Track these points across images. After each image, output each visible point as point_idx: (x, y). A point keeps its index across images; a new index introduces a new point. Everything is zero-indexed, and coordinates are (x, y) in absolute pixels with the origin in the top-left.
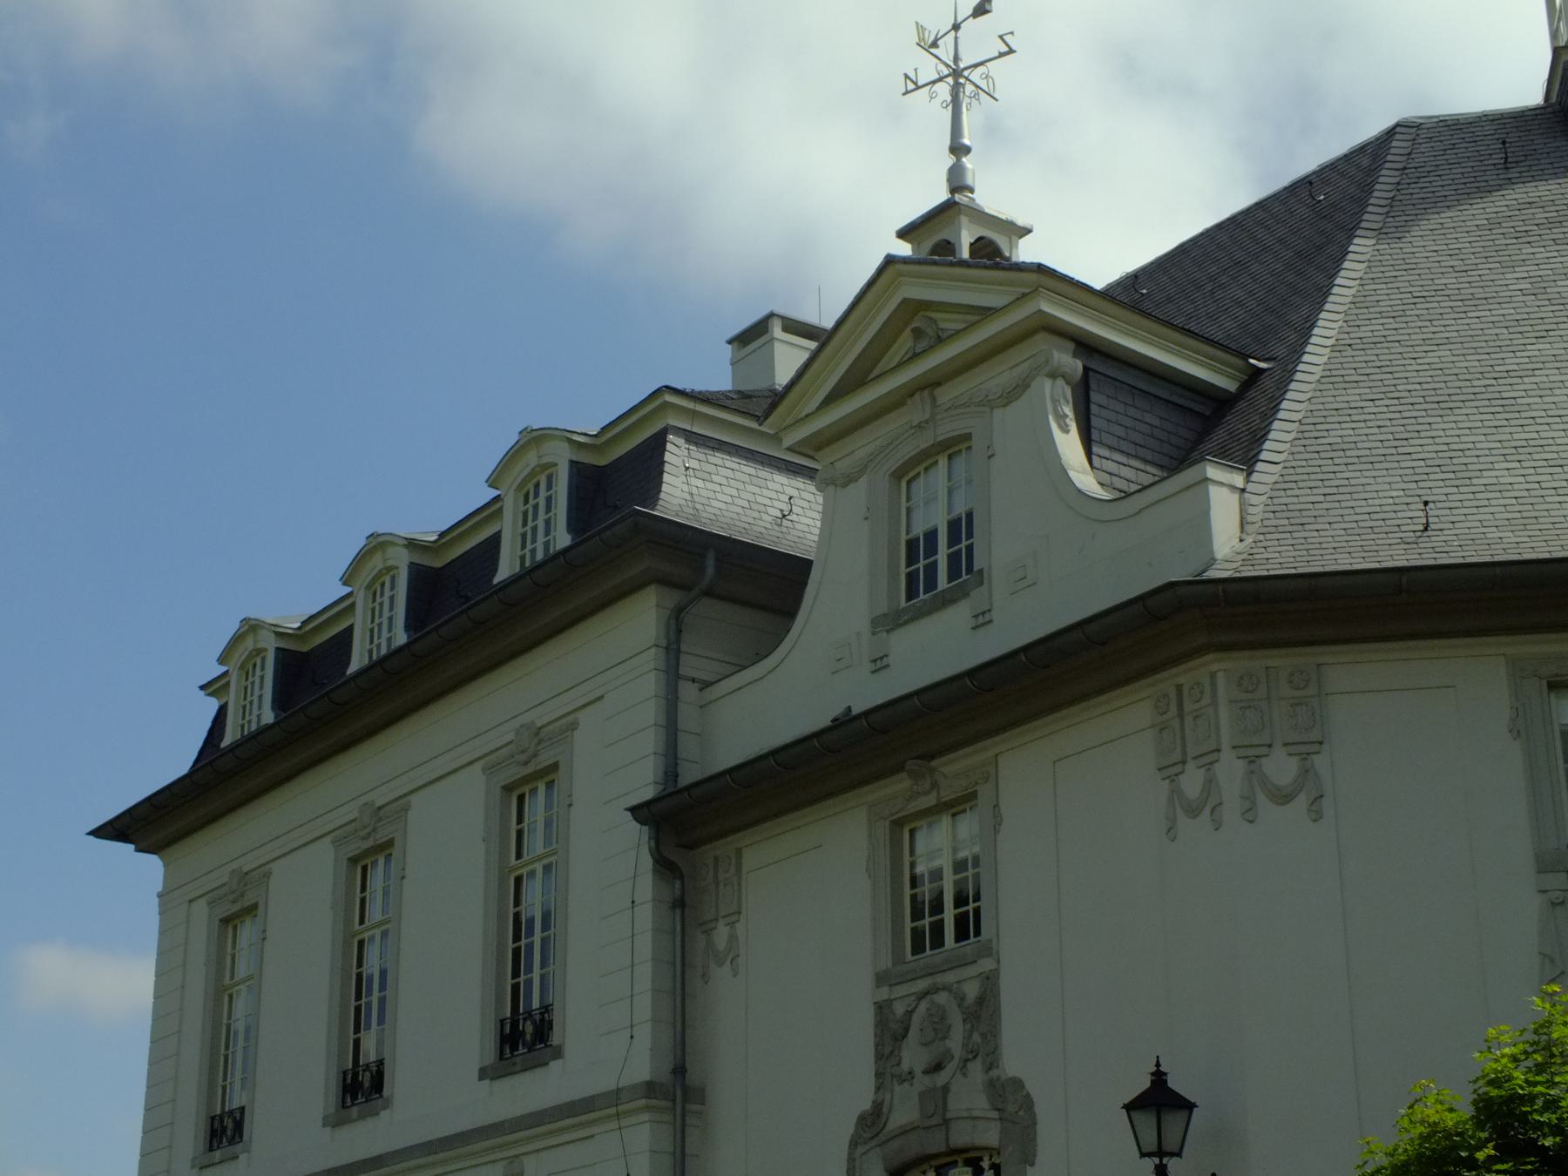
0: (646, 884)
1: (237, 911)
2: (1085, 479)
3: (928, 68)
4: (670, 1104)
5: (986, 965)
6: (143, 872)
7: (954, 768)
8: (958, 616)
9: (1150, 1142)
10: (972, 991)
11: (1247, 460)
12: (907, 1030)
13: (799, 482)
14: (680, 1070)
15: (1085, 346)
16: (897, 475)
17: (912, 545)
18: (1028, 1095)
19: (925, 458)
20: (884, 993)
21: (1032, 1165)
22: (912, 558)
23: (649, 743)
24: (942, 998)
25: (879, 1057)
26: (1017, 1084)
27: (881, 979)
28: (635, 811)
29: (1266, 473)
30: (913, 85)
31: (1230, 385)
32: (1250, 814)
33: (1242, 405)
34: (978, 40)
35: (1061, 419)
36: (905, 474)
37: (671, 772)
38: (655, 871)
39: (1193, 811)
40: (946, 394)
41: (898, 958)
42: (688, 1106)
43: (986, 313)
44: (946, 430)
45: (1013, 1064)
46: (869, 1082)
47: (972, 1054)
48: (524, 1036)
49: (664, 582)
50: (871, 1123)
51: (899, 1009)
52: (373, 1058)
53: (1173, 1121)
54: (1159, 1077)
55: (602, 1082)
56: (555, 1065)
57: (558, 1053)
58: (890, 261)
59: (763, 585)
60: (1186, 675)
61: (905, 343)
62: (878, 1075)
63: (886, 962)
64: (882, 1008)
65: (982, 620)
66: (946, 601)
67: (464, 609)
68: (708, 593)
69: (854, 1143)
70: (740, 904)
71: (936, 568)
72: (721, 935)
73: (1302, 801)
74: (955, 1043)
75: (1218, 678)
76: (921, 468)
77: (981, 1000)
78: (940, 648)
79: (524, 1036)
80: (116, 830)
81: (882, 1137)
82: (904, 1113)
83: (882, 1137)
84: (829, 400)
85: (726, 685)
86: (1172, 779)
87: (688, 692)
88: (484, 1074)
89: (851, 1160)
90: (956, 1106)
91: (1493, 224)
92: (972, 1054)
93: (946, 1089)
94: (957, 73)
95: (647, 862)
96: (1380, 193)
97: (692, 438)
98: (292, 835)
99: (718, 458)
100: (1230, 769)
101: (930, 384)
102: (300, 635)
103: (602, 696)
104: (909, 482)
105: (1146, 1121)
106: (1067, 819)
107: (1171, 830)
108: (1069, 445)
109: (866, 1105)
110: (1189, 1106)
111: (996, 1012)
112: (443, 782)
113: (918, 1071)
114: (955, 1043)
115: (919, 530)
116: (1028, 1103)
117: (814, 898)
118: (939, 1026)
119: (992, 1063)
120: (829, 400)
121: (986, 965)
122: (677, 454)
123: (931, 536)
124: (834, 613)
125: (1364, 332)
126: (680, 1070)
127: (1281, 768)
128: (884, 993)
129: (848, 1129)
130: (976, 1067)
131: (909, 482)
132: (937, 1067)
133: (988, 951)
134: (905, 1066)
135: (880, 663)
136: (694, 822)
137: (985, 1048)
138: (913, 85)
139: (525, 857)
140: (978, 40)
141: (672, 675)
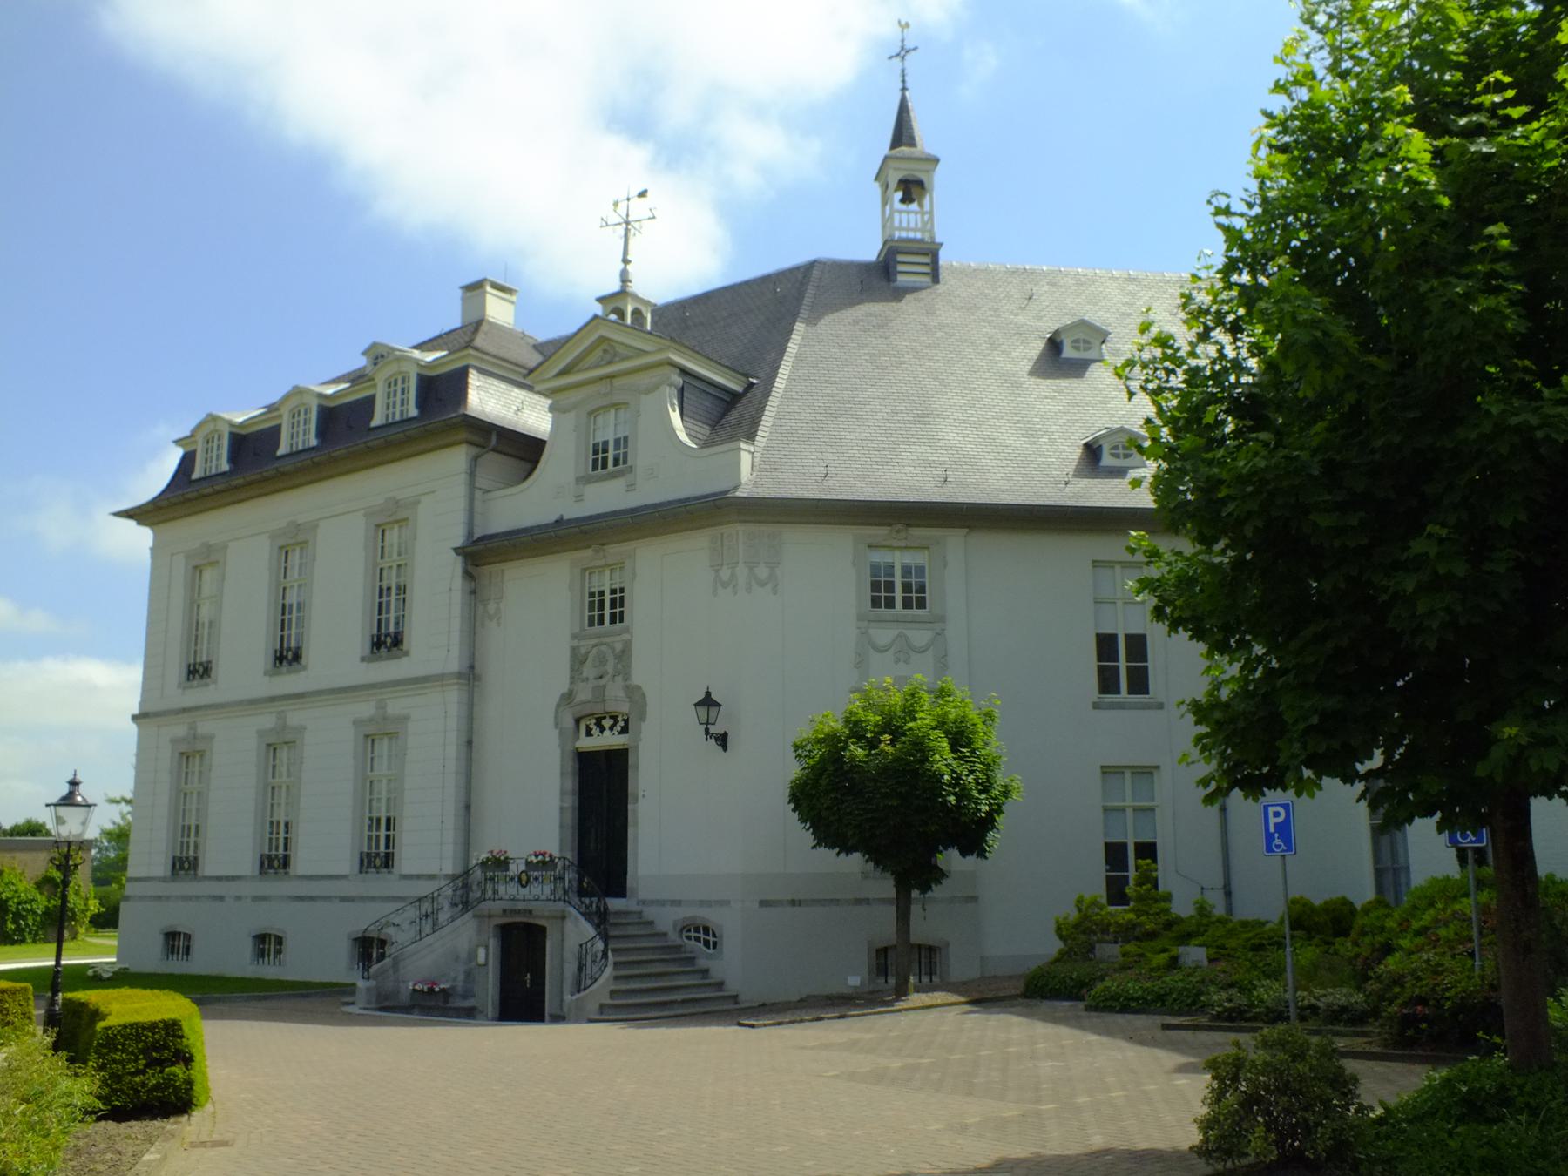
0: (458, 581)
1: (203, 563)
2: (683, 436)
3: (614, 218)
5: (626, 637)
6: (141, 538)
7: (614, 551)
8: (618, 485)
9: (704, 720)
10: (618, 647)
11: (751, 437)
13: (524, 393)
14: (472, 667)
15: (684, 372)
16: (590, 414)
17: (595, 446)
19: (605, 408)
20: (576, 643)
22: (596, 452)
23: (461, 517)
24: (603, 648)
25: (572, 670)
26: (639, 688)
27: (574, 637)
28: (455, 549)
29: (760, 441)
30: (605, 224)
31: (738, 388)
32: (749, 589)
33: (744, 400)
34: (638, 209)
35: (673, 405)
36: (594, 413)
37: (470, 533)
39: (725, 585)
40: (617, 382)
41: (583, 629)
43: (646, 352)
44: (616, 399)
45: (636, 679)
47: (617, 673)
48: (387, 642)
49: (470, 443)
50: (567, 698)
51: (583, 651)
52: (293, 644)
53: (713, 710)
54: (708, 694)
55: (435, 669)
56: (405, 659)
57: (407, 654)
58: (596, 317)
59: (524, 451)
60: (725, 529)
61: (598, 353)
62: (572, 678)
63: (577, 630)
64: (574, 650)
65: (631, 488)
66: (613, 476)
67: (346, 432)
68: (494, 450)
69: (558, 706)
71: (605, 460)
72: (492, 607)
73: (769, 586)
74: (610, 668)
75: (738, 533)
77: (623, 651)
78: (608, 497)
79: (387, 642)
80: (134, 515)
82: (584, 693)
84: (564, 372)
85: (498, 493)
86: (717, 571)
87: (478, 494)
88: (363, 659)
90: (609, 693)
91: (856, 323)
92: (617, 673)
93: (604, 687)
94: (627, 223)
96: (807, 300)
97: (481, 371)
98: (246, 530)
99: (491, 380)
100: (742, 572)
101: (611, 377)
102: (242, 425)
103: (437, 488)
105: (703, 710)
106: (660, 576)
107: (715, 593)
108: (675, 417)
109: (565, 689)
110: (719, 705)
111: (630, 656)
114: (610, 668)
115: (599, 439)
116: (644, 696)
117: (541, 598)
118: (602, 660)
119: (627, 677)
120: (564, 372)
121: (626, 637)
122: (474, 379)
123: (606, 443)
124: (557, 469)
125: (800, 373)
126: (472, 667)
127: (762, 572)
128: (576, 643)
129: (557, 698)
130: (619, 679)
133: (627, 630)
134: (585, 675)
135: (579, 498)
136: (482, 554)
137: (624, 670)
138: (605, 224)
140: (638, 209)
141: (472, 486)
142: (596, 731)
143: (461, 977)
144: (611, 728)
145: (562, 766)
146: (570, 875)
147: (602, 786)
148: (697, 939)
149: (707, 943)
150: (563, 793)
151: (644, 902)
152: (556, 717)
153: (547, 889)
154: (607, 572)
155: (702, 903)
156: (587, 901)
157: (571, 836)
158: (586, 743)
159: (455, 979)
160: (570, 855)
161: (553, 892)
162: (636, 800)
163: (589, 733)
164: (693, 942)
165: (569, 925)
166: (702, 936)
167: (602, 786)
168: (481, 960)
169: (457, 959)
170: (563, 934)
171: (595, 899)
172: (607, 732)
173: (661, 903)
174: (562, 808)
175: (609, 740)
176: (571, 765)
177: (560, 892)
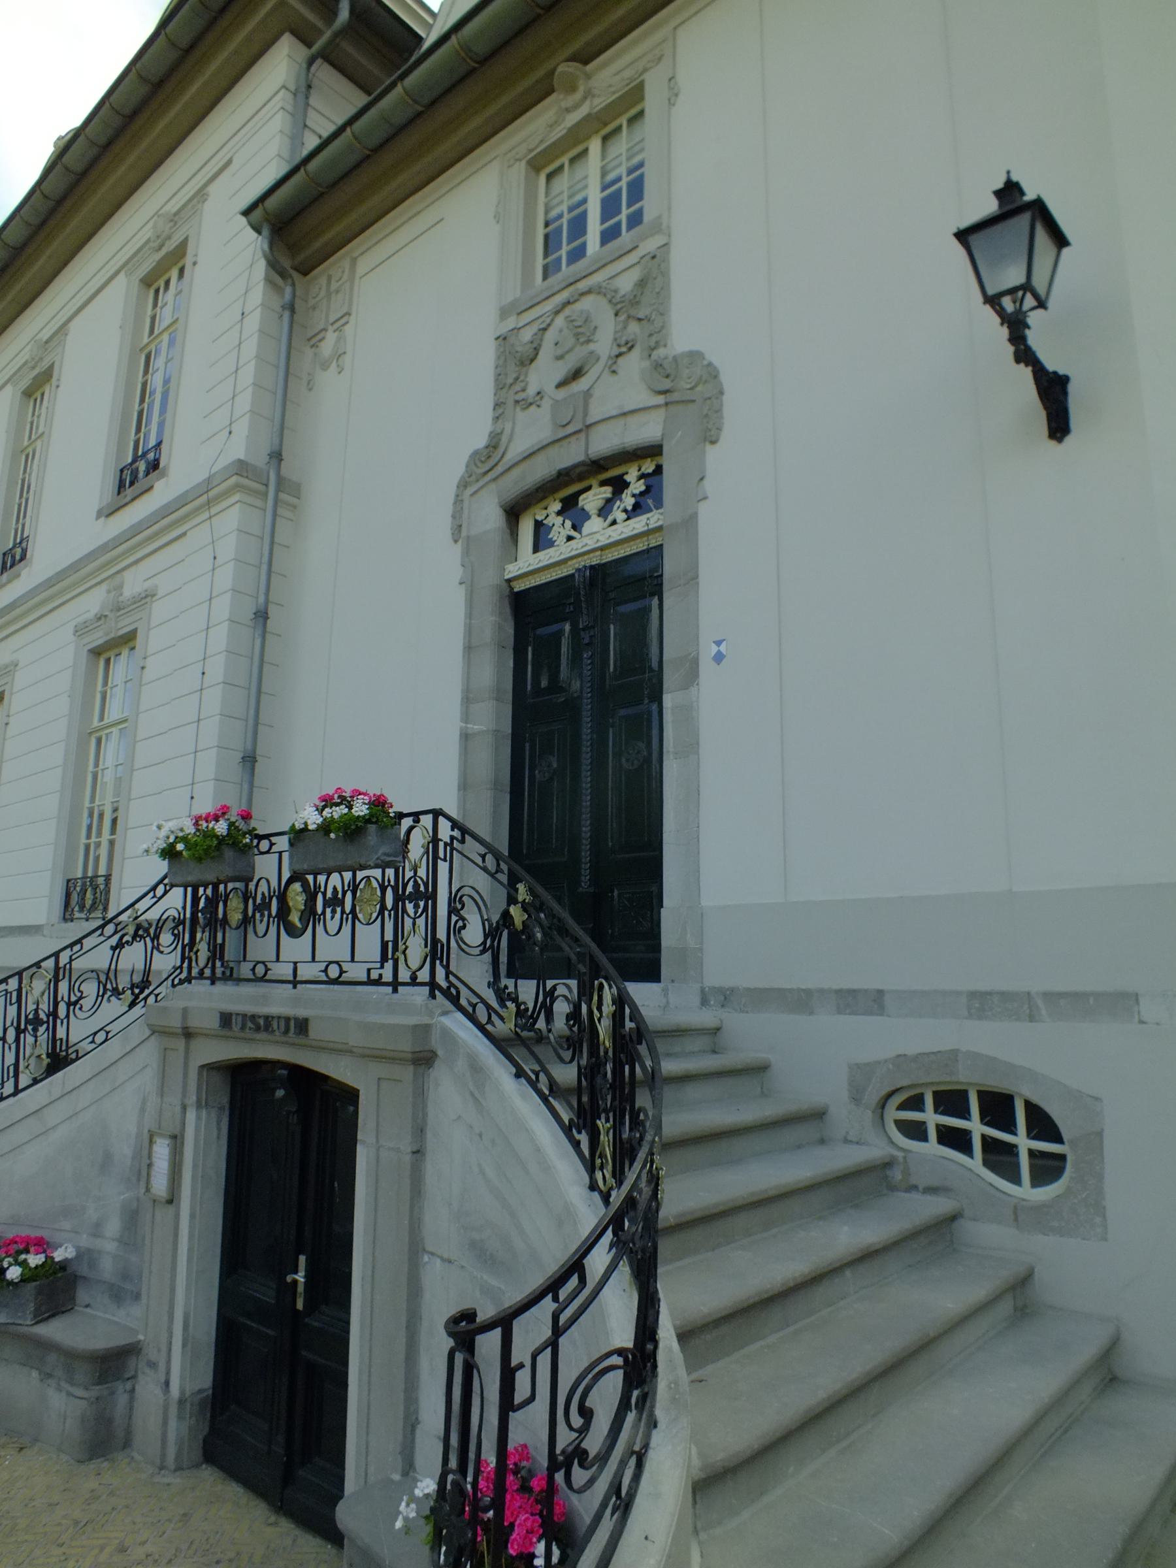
4: (263, 488)
5: (650, 245)
10: (626, 284)
12: (537, 351)
14: (277, 456)
18: (710, 364)
21: (713, 442)
24: (587, 303)
25: (500, 386)
38: (268, 280)
42: (282, 496)
46: (489, 414)
50: (487, 460)
51: (527, 335)
62: (497, 405)
69: (463, 484)
70: (350, 304)
76: (565, 160)
81: (499, 469)
82: (530, 430)
83: (499, 469)
89: (458, 500)
93: (588, 394)
95: (261, 265)
104: (550, 177)
109: (481, 442)
112: (49, 616)
113: (550, 388)
119: (657, 337)
126: (277, 456)
129: (458, 469)
130: (634, 363)
131: (550, 177)
132: (577, 374)
134: (531, 391)
137: (642, 307)
139: (106, 721)
142: (560, 528)
143: (113, 1227)
144: (603, 512)
145: (469, 631)
146: (471, 878)
147: (584, 670)
148: (956, 1140)
149: (999, 1156)
150: (468, 699)
151: (726, 997)
152: (457, 515)
153: (369, 939)
154: (595, 145)
155: (982, 1004)
156: (527, 990)
157: (492, 762)
158: (528, 563)
159: (97, 1230)
160: (490, 819)
161: (390, 951)
162: (692, 674)
163: (541, 541)
164: (932, 1147)
165: (446, 1090)
166: (976, 1127)
167: (584, 670)
168: (160, 1184)
169: (106, 1162)
170: (420, 1131)
171: (566, 988)
172: (594, 525)
173: (801, 1001)
174: (465, 737)
175: (602, 533)
176: (494, 624)
177: (416, 948)
